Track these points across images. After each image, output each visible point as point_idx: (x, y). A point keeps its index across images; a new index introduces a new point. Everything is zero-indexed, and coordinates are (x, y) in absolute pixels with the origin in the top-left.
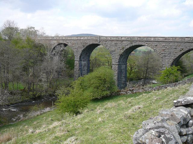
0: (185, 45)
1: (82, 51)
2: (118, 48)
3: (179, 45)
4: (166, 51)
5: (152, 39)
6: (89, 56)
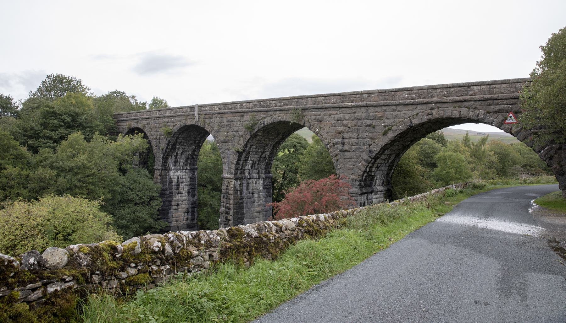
0: (396, 113)
2: (235, 133)
3: (379, 115)
4: (346, 135)
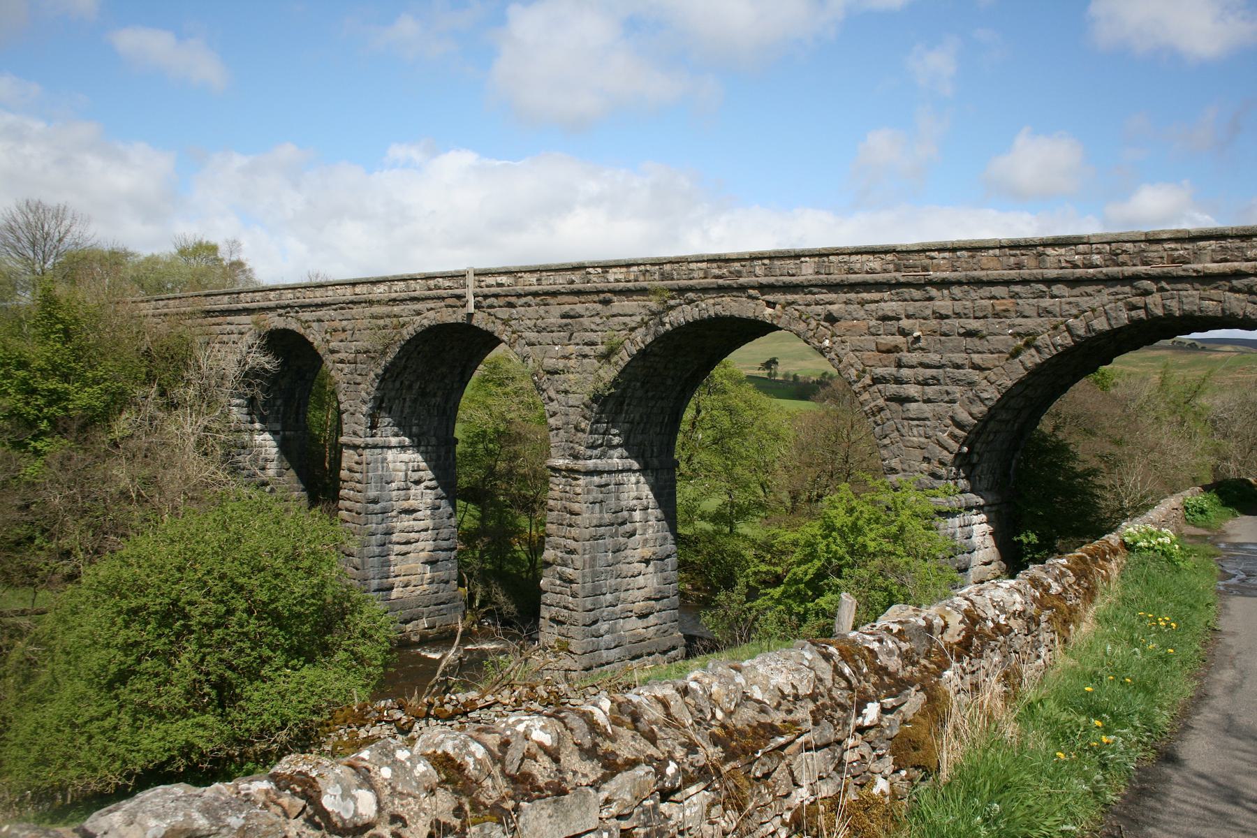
0: (1046, 302)
1: (383, 379)
4: (907, 357)
5: (807, 271)
6: (448, 414)
